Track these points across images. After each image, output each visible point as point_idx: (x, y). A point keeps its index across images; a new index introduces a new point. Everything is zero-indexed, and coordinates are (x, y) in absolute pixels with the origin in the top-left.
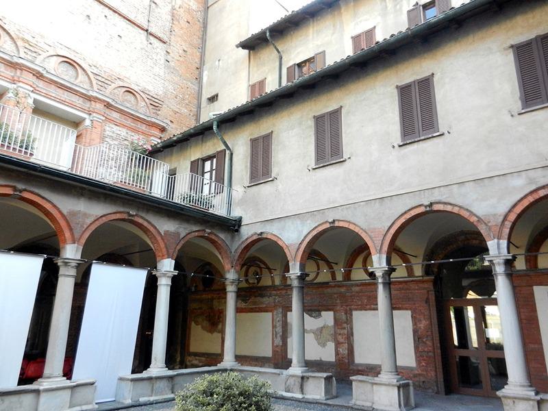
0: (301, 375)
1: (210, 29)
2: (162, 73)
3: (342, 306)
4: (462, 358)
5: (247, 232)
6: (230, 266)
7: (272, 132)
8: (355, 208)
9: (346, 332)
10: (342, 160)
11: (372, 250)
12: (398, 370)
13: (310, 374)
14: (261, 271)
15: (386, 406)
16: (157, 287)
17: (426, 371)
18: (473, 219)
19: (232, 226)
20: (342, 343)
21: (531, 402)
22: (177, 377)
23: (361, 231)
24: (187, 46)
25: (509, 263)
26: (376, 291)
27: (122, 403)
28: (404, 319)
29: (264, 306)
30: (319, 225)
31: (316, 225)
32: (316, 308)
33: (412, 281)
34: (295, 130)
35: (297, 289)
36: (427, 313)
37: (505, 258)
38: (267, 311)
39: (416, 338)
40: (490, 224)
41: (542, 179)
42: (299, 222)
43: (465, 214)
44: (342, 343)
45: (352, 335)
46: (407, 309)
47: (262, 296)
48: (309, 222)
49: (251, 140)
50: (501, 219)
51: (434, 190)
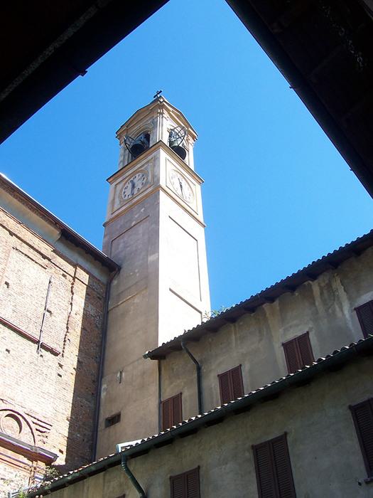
1: (112, 336)
2: (52, 390)
24: (83, 356)
34: (228, 465)
49: (171, 478)
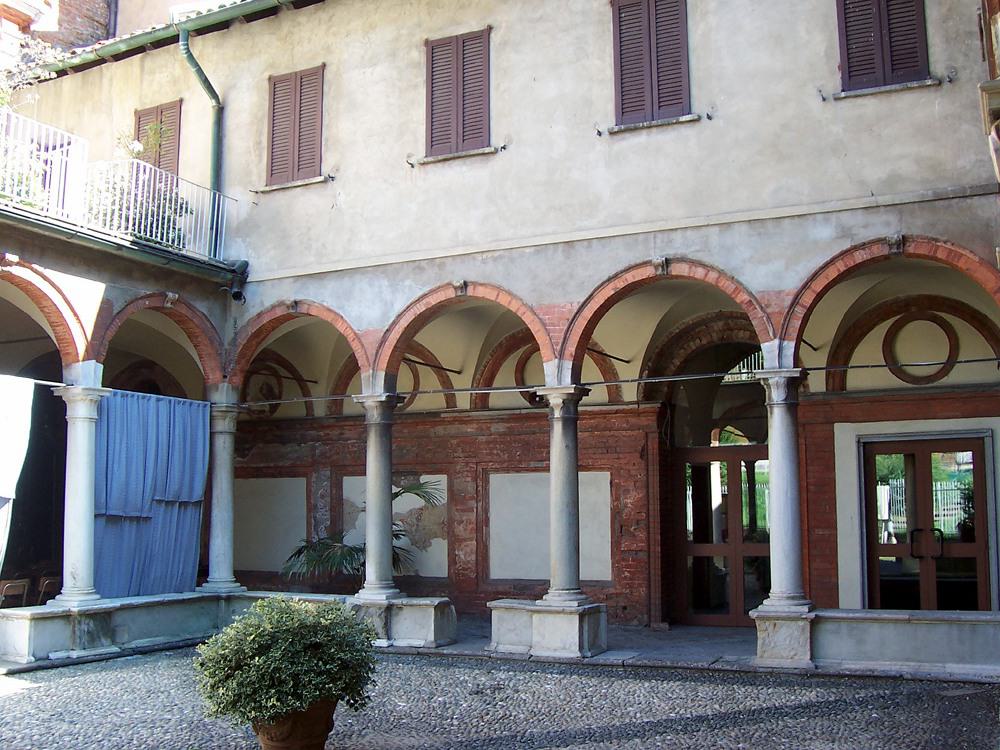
0: (386, 602)
3: (467, 463)
4: (698, 561)
5: (265, 296)
6: (218, 375)
7: (324, 66)
8: (512, 260)
9: (473, 516)
10: (487, 150)
11: (545, 351)
12: (579, 586)
13: (405, 601)
14: (280, 384)
15: (555, 650)
16: (66, 423)
17: (630, 587)
18: (742, 297)
19: (230, 282)
20: (465, 540)
21: (801, 623)
22: (120, 613)
23: (523, 309)
25: (794, 385)
26: (548, 433)
27: (17, 663)
28: (597, 489)
29: (288, 463)
30: (432, 292)
31: (426, 290)
32: (409, 467)
33: (617, 412)
35: (378, 428)
36: (641, 477)
37: (788, 375)
38: (294, 476)
39: (617, 526)
40: (769, 310)
41: (862, 231)
42: (385, 283)
43: (728, 287)
44: (465, 540)
45: (487, 525)
46: (601, 469)
47: (283, 442)
48: (408, 283)
49: (270, 79)
50: (788, 301)
51: (674, 235)
